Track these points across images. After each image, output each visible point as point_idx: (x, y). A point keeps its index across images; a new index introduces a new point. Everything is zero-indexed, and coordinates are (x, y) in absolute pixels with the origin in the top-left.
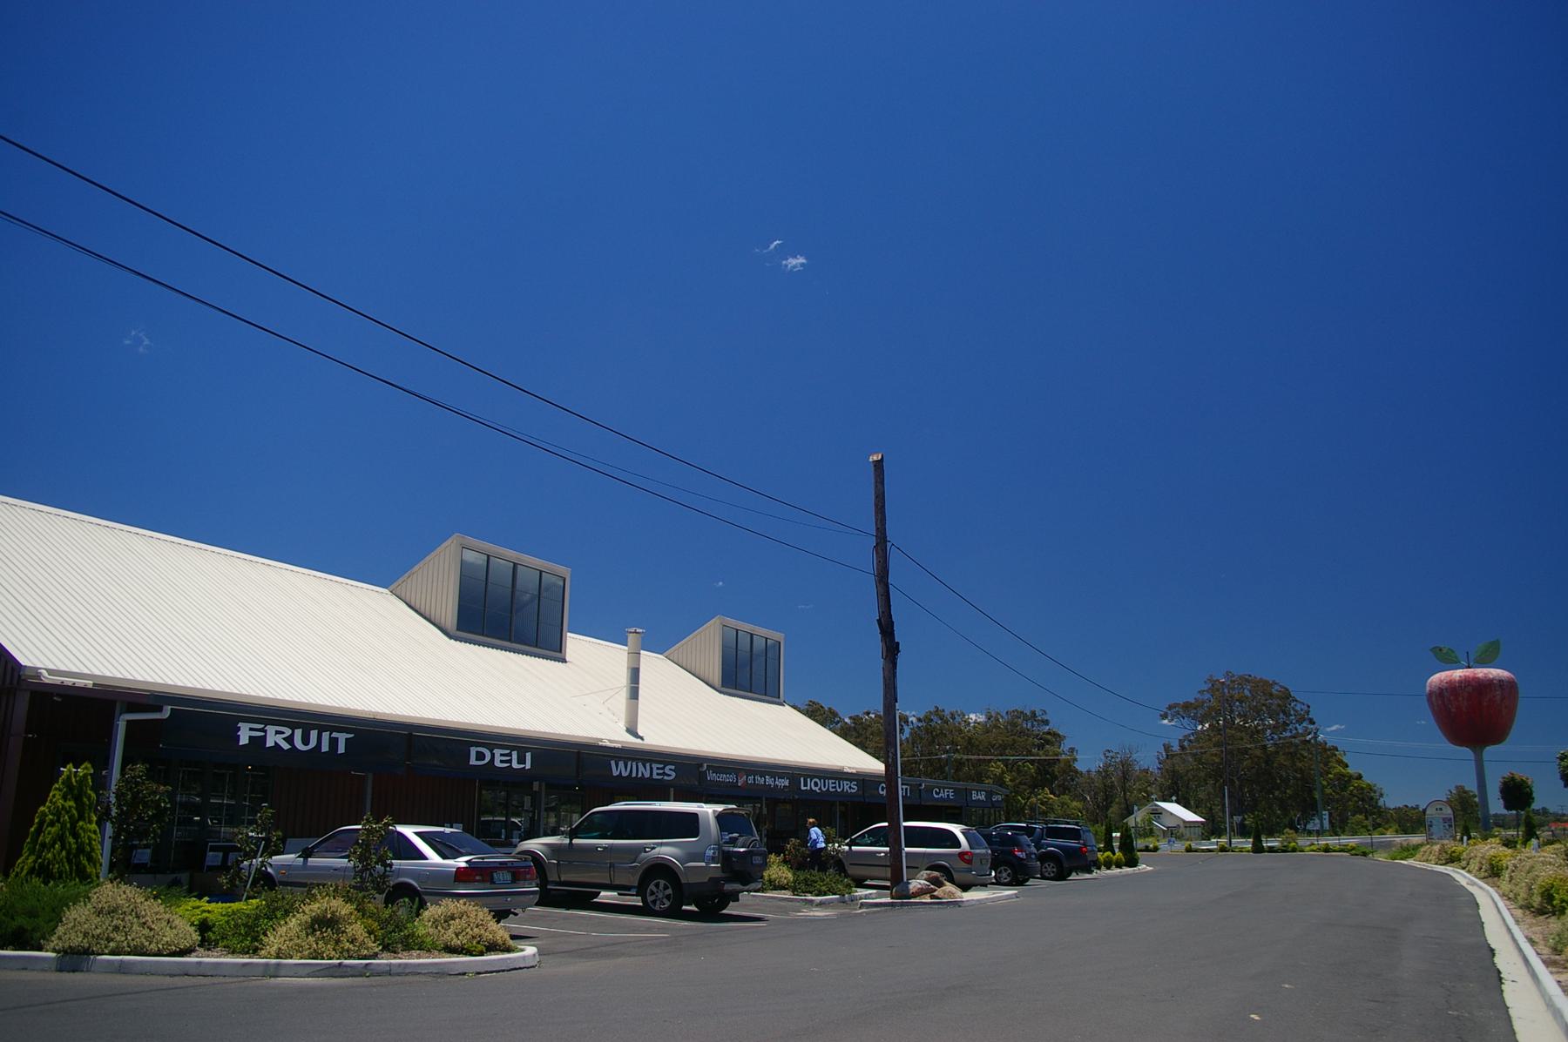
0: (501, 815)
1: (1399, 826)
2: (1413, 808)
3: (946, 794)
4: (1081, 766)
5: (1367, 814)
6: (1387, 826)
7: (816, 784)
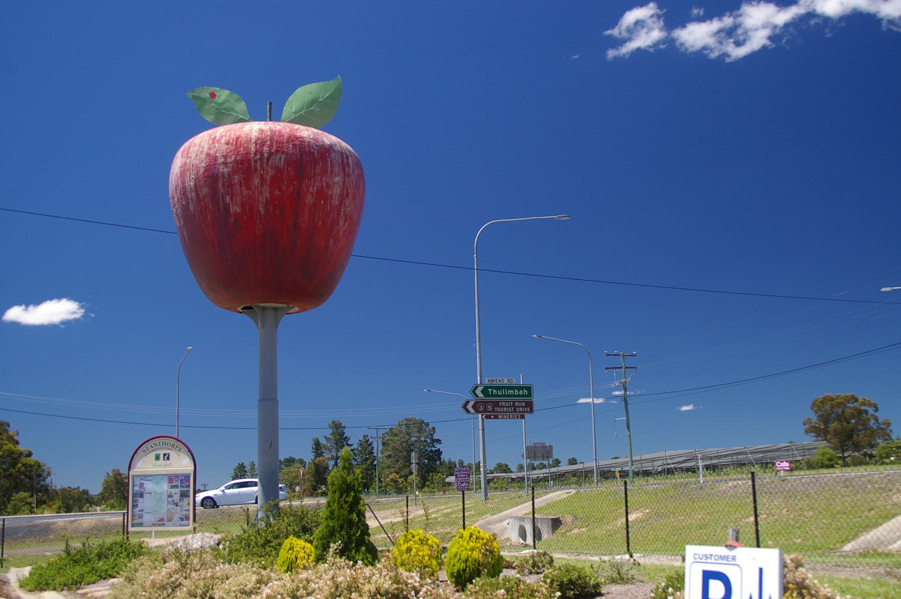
1: (63, 503)
2: (75, 489)
5: (32, 490)
6: (50, 503)
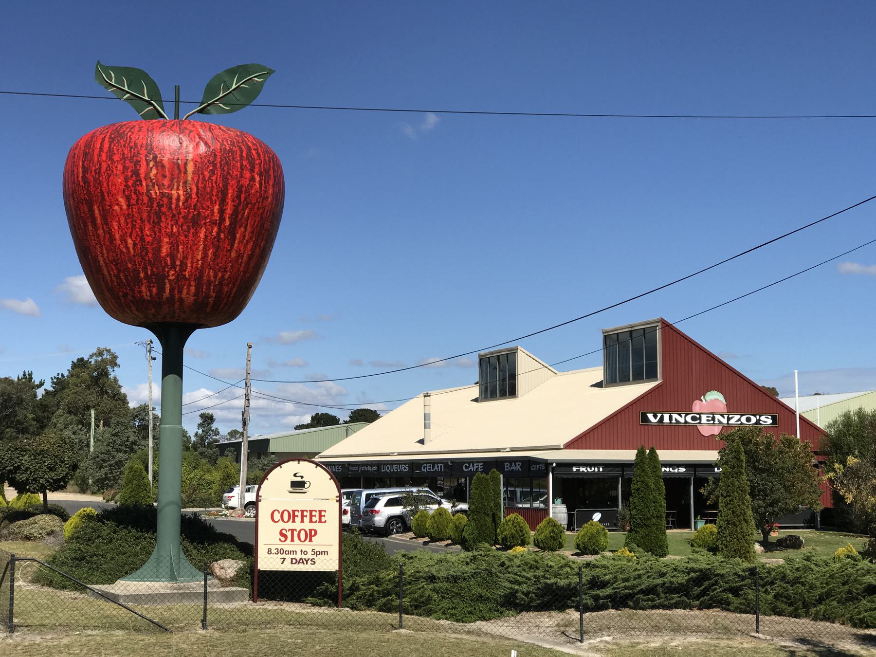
0: (537, 489)
3: (475, 467)
4: (129, 405)
7: (388, 468)
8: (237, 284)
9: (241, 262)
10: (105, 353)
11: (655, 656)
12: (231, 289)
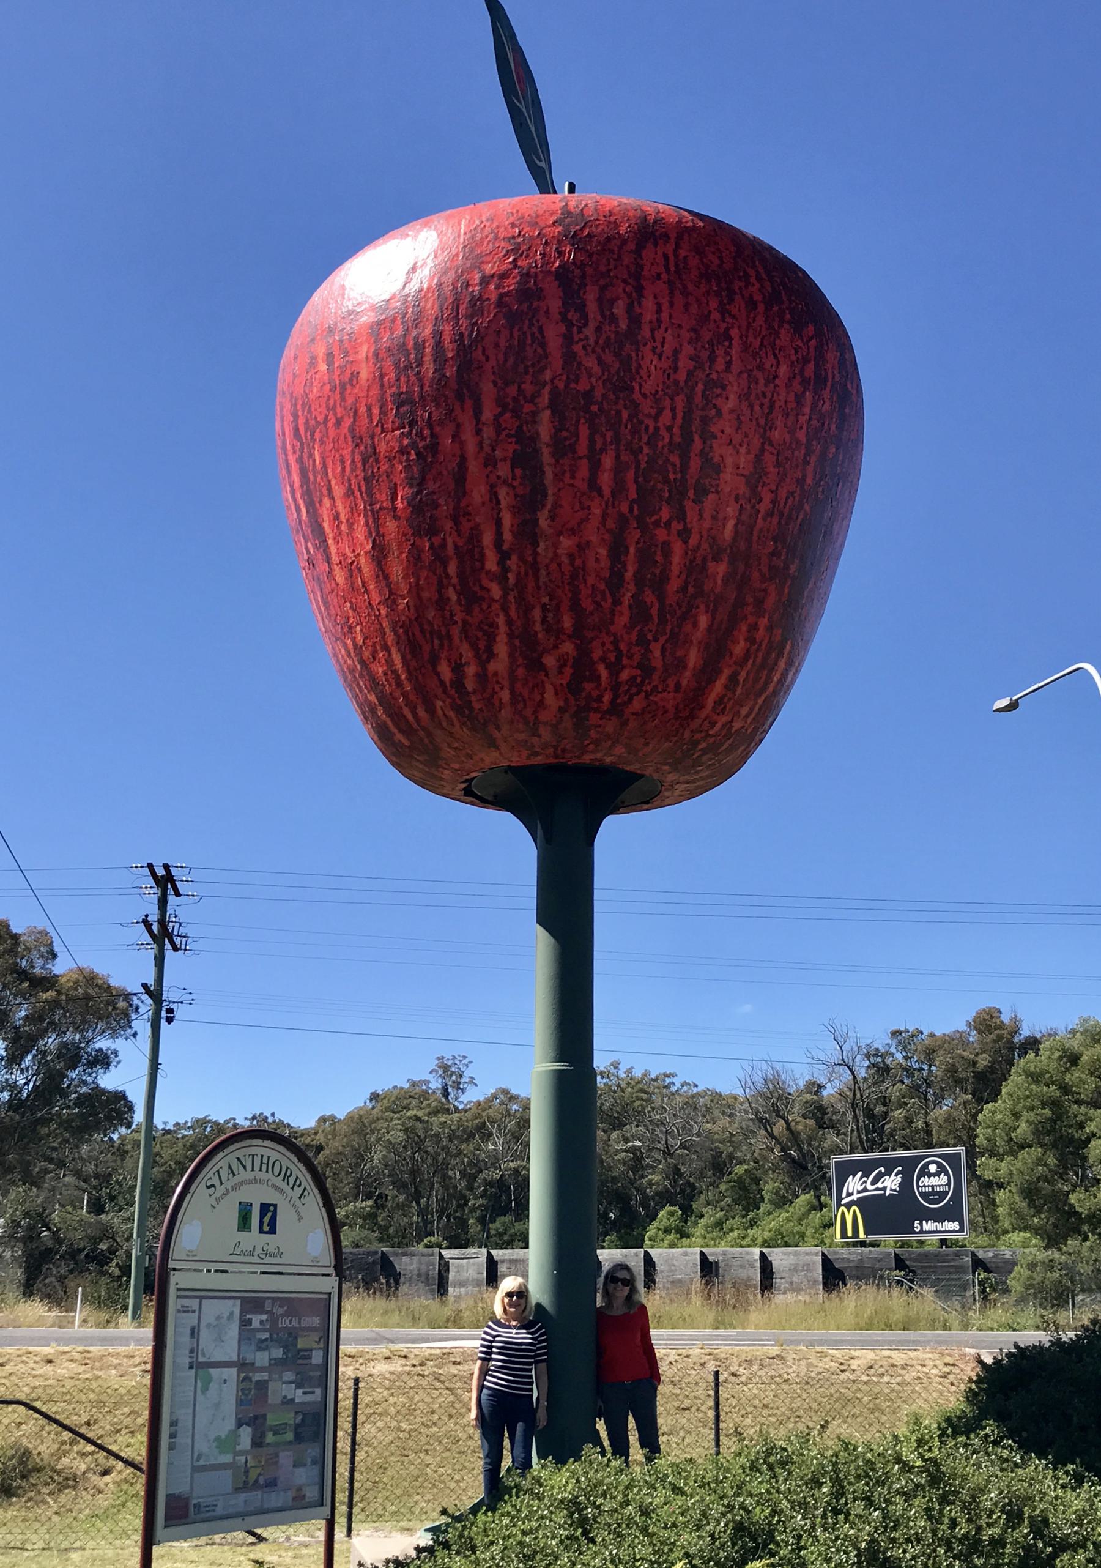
8: (390, 637)
9: (363, 583)
10: (884, 1109)
11: (660, 1564)
12: (389, 662)
